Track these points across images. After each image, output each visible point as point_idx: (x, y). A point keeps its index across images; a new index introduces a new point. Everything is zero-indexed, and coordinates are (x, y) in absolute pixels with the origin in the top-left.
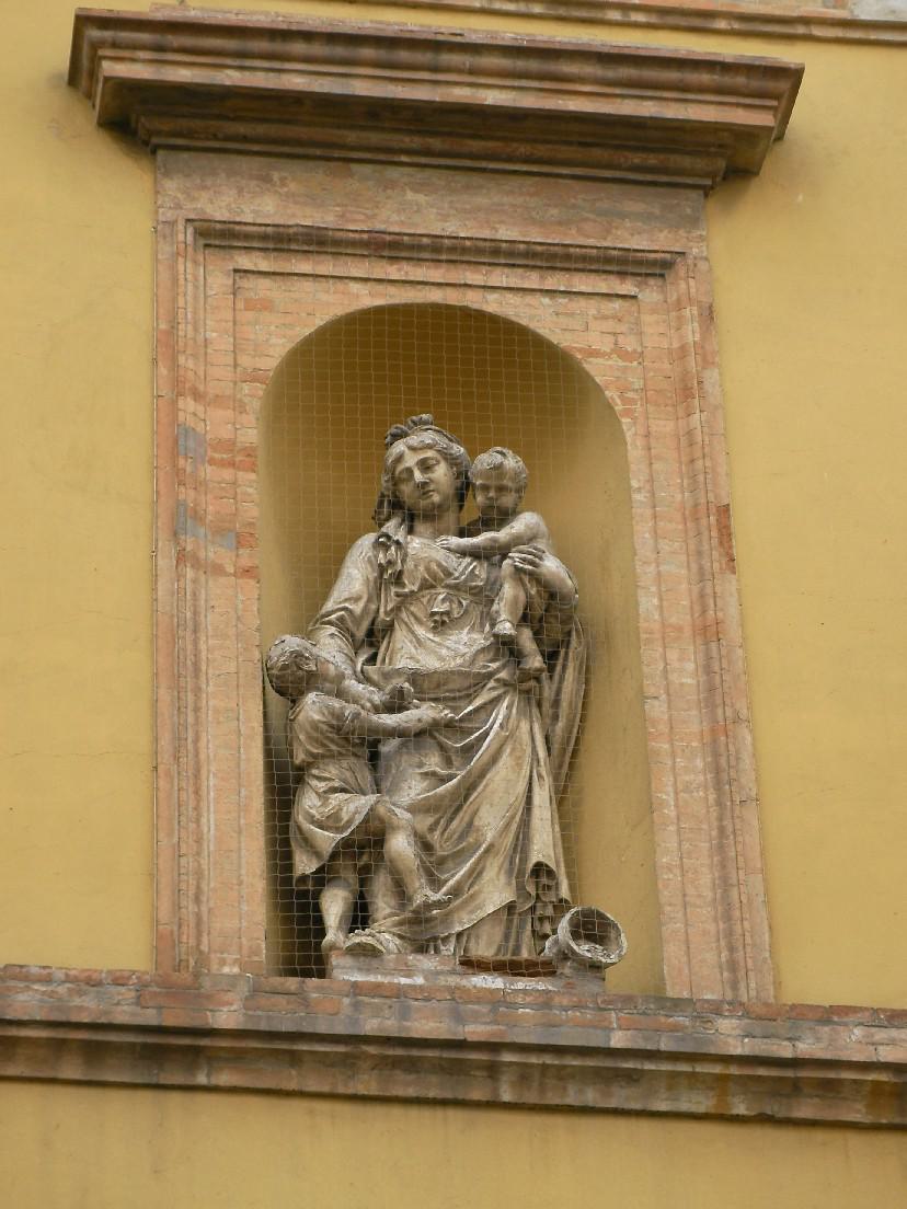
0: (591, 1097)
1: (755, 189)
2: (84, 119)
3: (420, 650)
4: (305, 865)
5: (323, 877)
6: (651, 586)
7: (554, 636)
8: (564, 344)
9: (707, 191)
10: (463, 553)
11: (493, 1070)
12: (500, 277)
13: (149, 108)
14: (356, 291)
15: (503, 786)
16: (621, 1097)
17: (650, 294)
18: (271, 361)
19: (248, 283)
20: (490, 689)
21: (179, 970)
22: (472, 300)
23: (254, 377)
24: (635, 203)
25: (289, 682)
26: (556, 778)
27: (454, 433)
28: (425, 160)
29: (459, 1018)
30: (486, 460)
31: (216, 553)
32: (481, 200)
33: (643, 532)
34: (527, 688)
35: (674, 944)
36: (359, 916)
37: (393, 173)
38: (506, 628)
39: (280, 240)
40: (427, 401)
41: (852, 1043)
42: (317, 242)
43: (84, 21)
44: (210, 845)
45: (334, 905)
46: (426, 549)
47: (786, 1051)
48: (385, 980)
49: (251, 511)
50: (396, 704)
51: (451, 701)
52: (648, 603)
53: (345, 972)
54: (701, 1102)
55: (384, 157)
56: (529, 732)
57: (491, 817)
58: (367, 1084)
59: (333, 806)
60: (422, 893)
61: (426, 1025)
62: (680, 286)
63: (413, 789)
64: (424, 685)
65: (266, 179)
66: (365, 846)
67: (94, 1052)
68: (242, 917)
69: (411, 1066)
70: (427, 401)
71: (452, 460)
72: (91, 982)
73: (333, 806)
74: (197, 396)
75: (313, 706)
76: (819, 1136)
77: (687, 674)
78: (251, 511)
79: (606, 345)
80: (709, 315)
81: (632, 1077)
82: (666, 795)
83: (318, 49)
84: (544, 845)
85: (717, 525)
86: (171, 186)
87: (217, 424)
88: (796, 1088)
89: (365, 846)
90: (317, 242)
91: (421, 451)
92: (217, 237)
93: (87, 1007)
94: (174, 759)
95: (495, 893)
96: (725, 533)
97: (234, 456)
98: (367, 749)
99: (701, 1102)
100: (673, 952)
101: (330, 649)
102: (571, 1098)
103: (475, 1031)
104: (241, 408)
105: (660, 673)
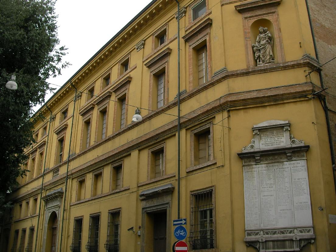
0: (273, 71)
1: (281, 5)
2: (237, 12)
3: (263, 42)
4: (256, 59)
5: (257, 59)
6: (276, 36)
7: (271, 39)
8: (269, 19)
9: (277, 6)
10: (264, 35)
11: (267, 70)
12: (264, 16)
13: (241, 11)
14: (256, 19)
15: (268, 50)
16: (275, 70)
17: (274, 14)
18: (250, 26)
19: (248, 21)
20: (54, 89)
21: (248, 67)
22: (263, 18)
23: (249, 27)
24: (272, 8)
25: (253, 47)
26: (272, 48)
27: (263, 27)
28: (258, 9)
29: (264, 67)
30: (265, 29)
31: (248, 40)
32: (262, 11)
33: (275, 31)
34: (269, 43)
35: (279, 59)
36: (260, 61)
37: (257, 10)
38: (267, 40)
39: (250, 17)
40: (262, 25)
41: (289, 64)
42: (252, 17)
43: (235, 6)
44: (249, 59)
45: (258, 61)
46: (262, 35)
47: (285, 65)
48: (261, 65)
49: (250, 36)
50: (260, 47)
51: (264, 46)
52: (275, 36)
53: (258, 66)
54: (280, 69)
55: (256, 10)
56: (270, 46)
57: (267, 53)
58: (260, 73)
59: (257, 54)
60: (263, 59)
61: (263, 68)
62: (276, 13)
63: (262, 52)
64: (262, 45)
65: (249, 13)
66: (259, 57)
67: (243, 74)
68: (252, 63)
69: (262, 71)
70: (262, 25)
71: (262, 29)
72: (242, 70)
73: (257, 54)
74: (246, 29)
75: (255, 48)
76: (288, 70)
77: (278, 41)
78: (250, 36)
79: (271, 19)
80: (278, 15)
81: (276, 69)
82: (278, 49)
83: (250, 4)
84: (271, 54)
85: (280, 30)
86: (243, 15)
87: (247, 31)
88: (286, 67)
89: (259, 57)
90: (252, 17)
91: (261, 29)
92: (246, 18)
93: (242, 72)
94: (247, 53)
95: (268, 57)
96: (280, 30)
97: (249, 33)
98: (259, 50)
99: (280, 69)
100: (279, 60)
101: (257, 44)
102: (272, 71)
103: (265, 68)
104: (249, 29)
105: (277, 41)
